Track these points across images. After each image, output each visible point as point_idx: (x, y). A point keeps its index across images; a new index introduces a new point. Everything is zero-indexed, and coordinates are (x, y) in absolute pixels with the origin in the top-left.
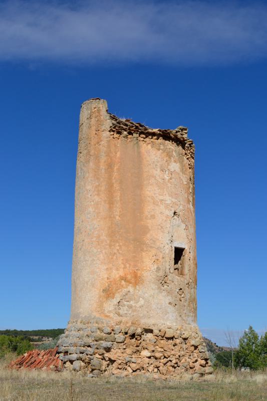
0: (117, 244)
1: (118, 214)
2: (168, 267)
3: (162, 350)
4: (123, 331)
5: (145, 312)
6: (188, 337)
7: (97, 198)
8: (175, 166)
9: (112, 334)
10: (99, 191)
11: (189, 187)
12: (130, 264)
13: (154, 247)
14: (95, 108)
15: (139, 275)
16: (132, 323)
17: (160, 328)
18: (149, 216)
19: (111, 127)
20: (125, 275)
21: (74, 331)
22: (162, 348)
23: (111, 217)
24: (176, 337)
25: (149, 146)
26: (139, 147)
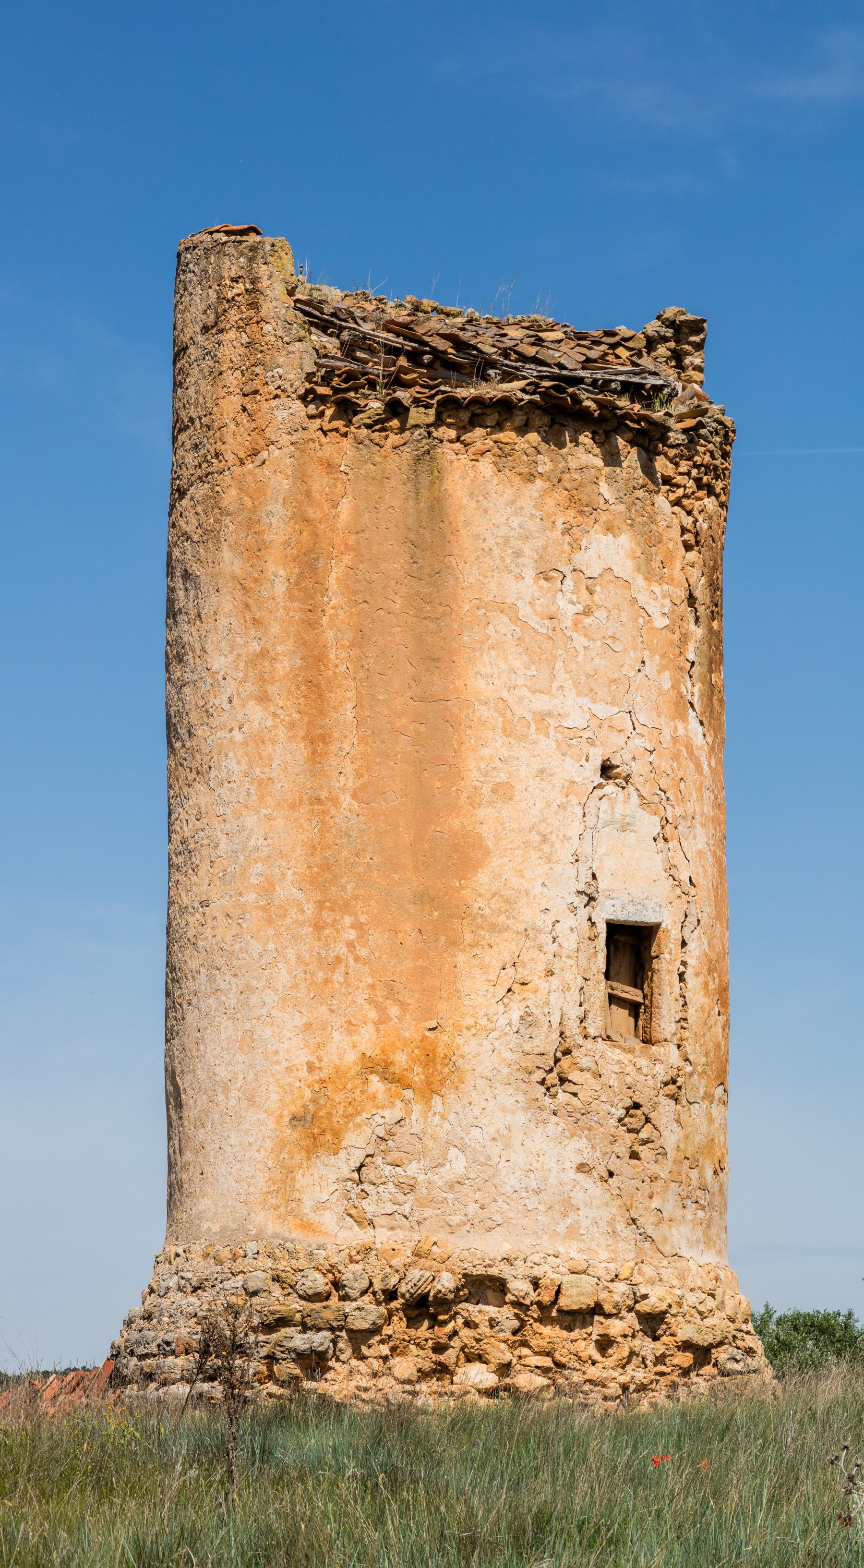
0: (348, 920)
1: (350, 784)
2: (576, 1012)
3: (547, 1362)
4: (377, 1286)
5: (472, 1208)
6: (664, 1307)
7: (256, 713)
8: (610, 551)
9: (334, 1301)
10: (261, 679)
11: (685, 638)
12: (403, 1005)
13: (507, 928)
14: (235, 280)
15: (441, 1051)
16: (417, 1254)
17: (537, 1272)
18: (486, 790)
19: (309, 377)
20: (383, 1051)
21: (180, 1289)
22: (548, 1354)
23: (318, 800)
24: (608, 1308)
25: (486, 466)
26: (437, 475)
